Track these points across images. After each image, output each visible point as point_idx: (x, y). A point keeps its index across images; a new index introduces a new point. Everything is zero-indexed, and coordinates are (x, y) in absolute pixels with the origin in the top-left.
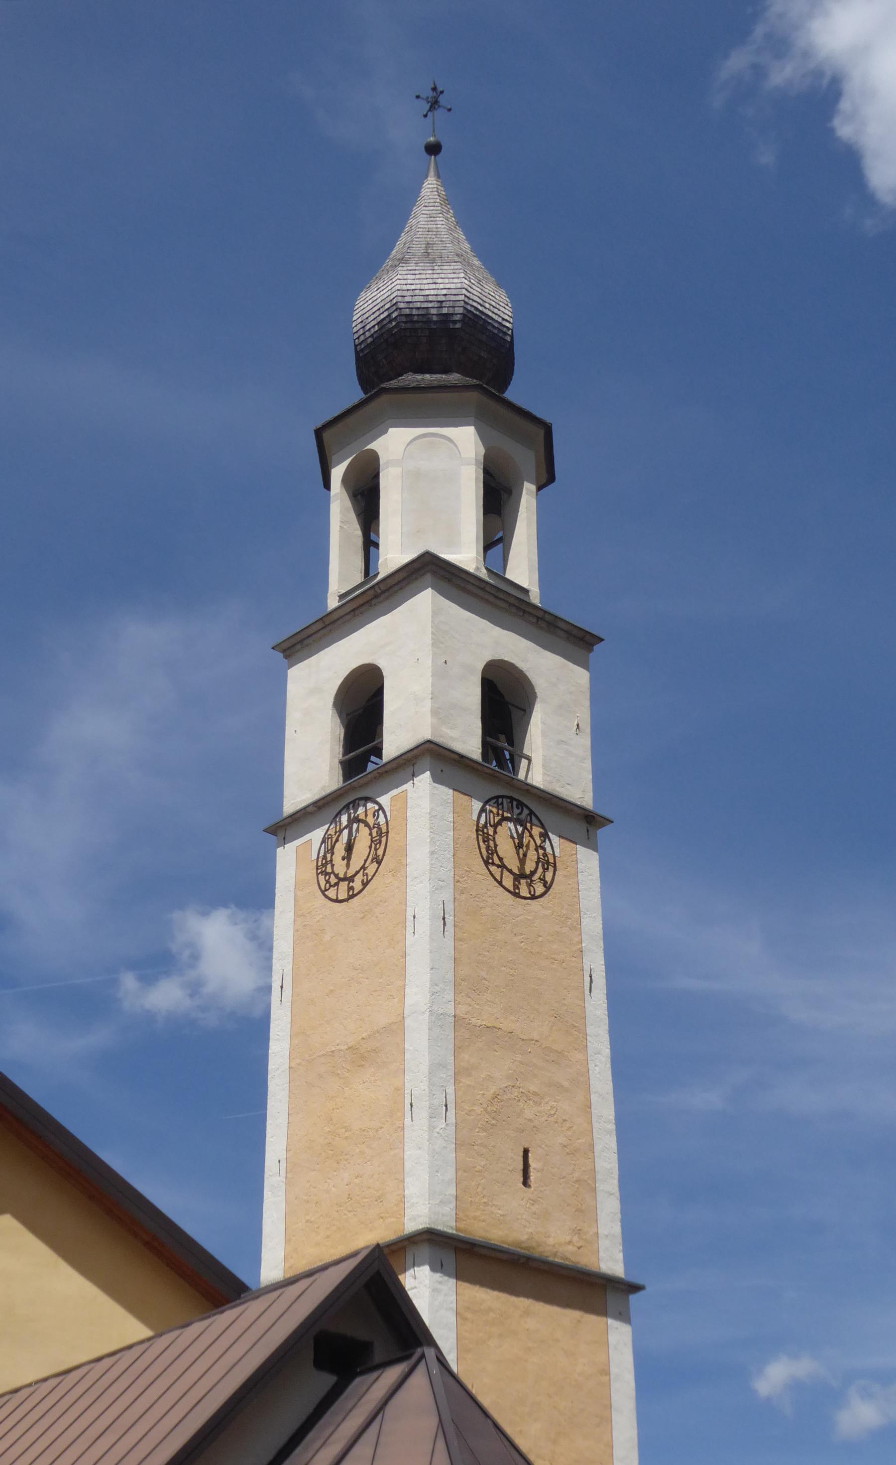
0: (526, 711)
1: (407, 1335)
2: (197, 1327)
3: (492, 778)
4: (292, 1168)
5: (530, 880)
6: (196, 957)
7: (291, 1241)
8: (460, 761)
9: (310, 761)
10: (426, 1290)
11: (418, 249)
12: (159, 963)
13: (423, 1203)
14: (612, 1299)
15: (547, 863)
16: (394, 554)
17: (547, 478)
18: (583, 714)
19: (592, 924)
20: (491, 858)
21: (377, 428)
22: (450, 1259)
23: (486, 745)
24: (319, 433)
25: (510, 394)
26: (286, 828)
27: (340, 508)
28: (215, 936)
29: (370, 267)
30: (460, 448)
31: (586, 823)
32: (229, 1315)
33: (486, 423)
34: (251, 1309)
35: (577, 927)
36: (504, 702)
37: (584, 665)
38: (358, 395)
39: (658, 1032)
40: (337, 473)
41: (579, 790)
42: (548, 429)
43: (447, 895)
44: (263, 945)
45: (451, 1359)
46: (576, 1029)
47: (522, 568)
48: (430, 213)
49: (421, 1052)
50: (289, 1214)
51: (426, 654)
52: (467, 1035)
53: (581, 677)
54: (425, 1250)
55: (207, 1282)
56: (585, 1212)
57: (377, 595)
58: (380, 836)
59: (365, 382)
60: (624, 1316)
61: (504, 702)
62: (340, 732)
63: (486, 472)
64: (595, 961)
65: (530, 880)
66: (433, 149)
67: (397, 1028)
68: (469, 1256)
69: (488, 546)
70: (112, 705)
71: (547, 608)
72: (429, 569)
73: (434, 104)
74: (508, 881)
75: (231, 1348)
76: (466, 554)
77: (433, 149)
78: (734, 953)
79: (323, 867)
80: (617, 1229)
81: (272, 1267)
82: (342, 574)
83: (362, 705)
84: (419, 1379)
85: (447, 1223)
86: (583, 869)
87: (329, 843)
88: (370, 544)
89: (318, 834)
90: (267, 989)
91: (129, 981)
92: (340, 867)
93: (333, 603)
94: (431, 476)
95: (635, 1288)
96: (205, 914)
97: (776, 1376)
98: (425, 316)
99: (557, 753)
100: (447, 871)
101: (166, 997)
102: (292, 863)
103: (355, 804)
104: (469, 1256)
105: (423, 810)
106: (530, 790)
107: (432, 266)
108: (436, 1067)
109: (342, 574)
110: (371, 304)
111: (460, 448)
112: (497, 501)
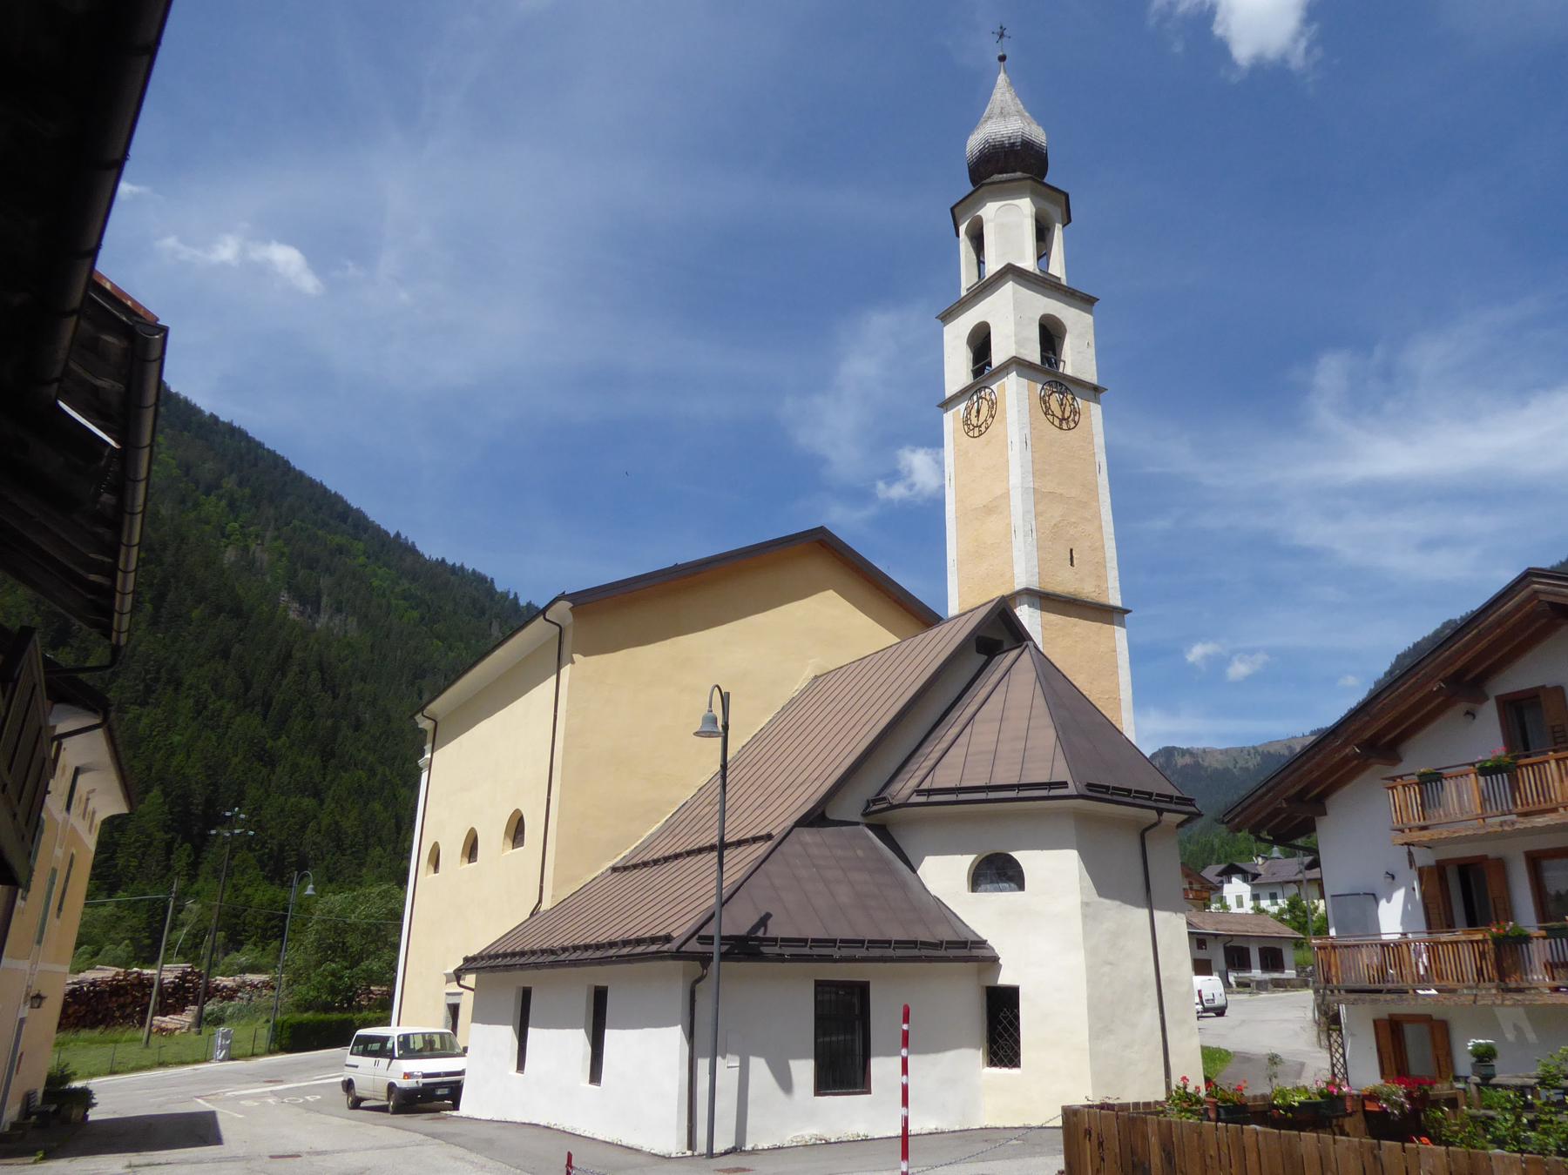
0: (1062, 338)
1: (1020, 637)
2: (921, 636)
3: (1046, 372)
4: (960, 563)
5: (1067, 421)
6: (910, 472)
7: (962, 596)
8: (1031, 365)
9: (957, 370)
10: (1026, 615)
11: (997, 111)
12: (893, 476)
13: (1023, 577)
14: (1116, 617)
15: (1075, 412)
16: (992, 266)
17: (1067, 220)
18: (1091, 338)
19: (1099, 440)
20: (1047, 411)
21: (981, 203)
22: (1037, 600)
23: (1042, 357)
24: (952, 210)
25: (1048, 180)
26: (947, 404)
27: (965, 245)
28: (918, 461)
29: (972, 126)
30: (1024, 207)
31: (1094, 391)
32: (936, 630)
33: (1035, 196)
34: (945, 628)
35: (1092, 442)
36: (1051, 335)
37: (1090, 313)
38: (971, 188)
39: (1135, 491)
40: (963, 229)
41: (1091, 376)
42: (1067, 196)
43: (1027, 431)
44: (940, 464)
45: (1040, 647)
46: (1093, 491)
47: (1057, 268)
48: (1002, 92)
49: (1018, 506)
50: (959, 585)
51: (1011, 320)
52: (1040, 496)
53: (1089, 318)
54: (1025, 598)
55: (924, 617)
56: (1101, 578)
57: (985, 287)
58: (993, 405)
59: (974, 182)
60: (1122, 624)
61: (1051, 335)
62: (971, 356)
63: (1037, 221)
64: (1101, 458)
65: (1067, 421)
66: (1002, 58)
67: (1006, 496)
68: (1046, 600)
69: (1039, 258)
70: (865, 357)
71: (1073, 286)
72: (1011, 272)
73: (1001, 35)
74: (1057, 422)
75: (936, 646)
76: (1028, 263)
77: (1002, 58)
78: (1175, 452)
79: (966, 421)
80: (1117, 585)
81: (953, 609)
82: (968, 278)
83: (980, 343)
84: (1026, 656)
85: (1035, 586)
86: (1093, 413)
87: (968, 410)
88: (981, 263)
89: (963, 406)
90: (943, 487)
91: (881, 485)
92: (974, 421)
93: (964, 293)
94: (1009, 223)
95: (1128, 612)
96: (913, 451)
97: (1197, 653)
98: (1002, 145)
99: (1079, 357)
100: (1026, 419)
101: (898, 491)
102: (951, 421)
103: (980, 390)
104: (1046, 600)
105: (1013, 392)
106: (1065, 377)
107: (1005, 119)
108: (1025, 513)
109: (968, 279)
110: (975, 142)
111: (1024, 207)
112: (1043, 234)
